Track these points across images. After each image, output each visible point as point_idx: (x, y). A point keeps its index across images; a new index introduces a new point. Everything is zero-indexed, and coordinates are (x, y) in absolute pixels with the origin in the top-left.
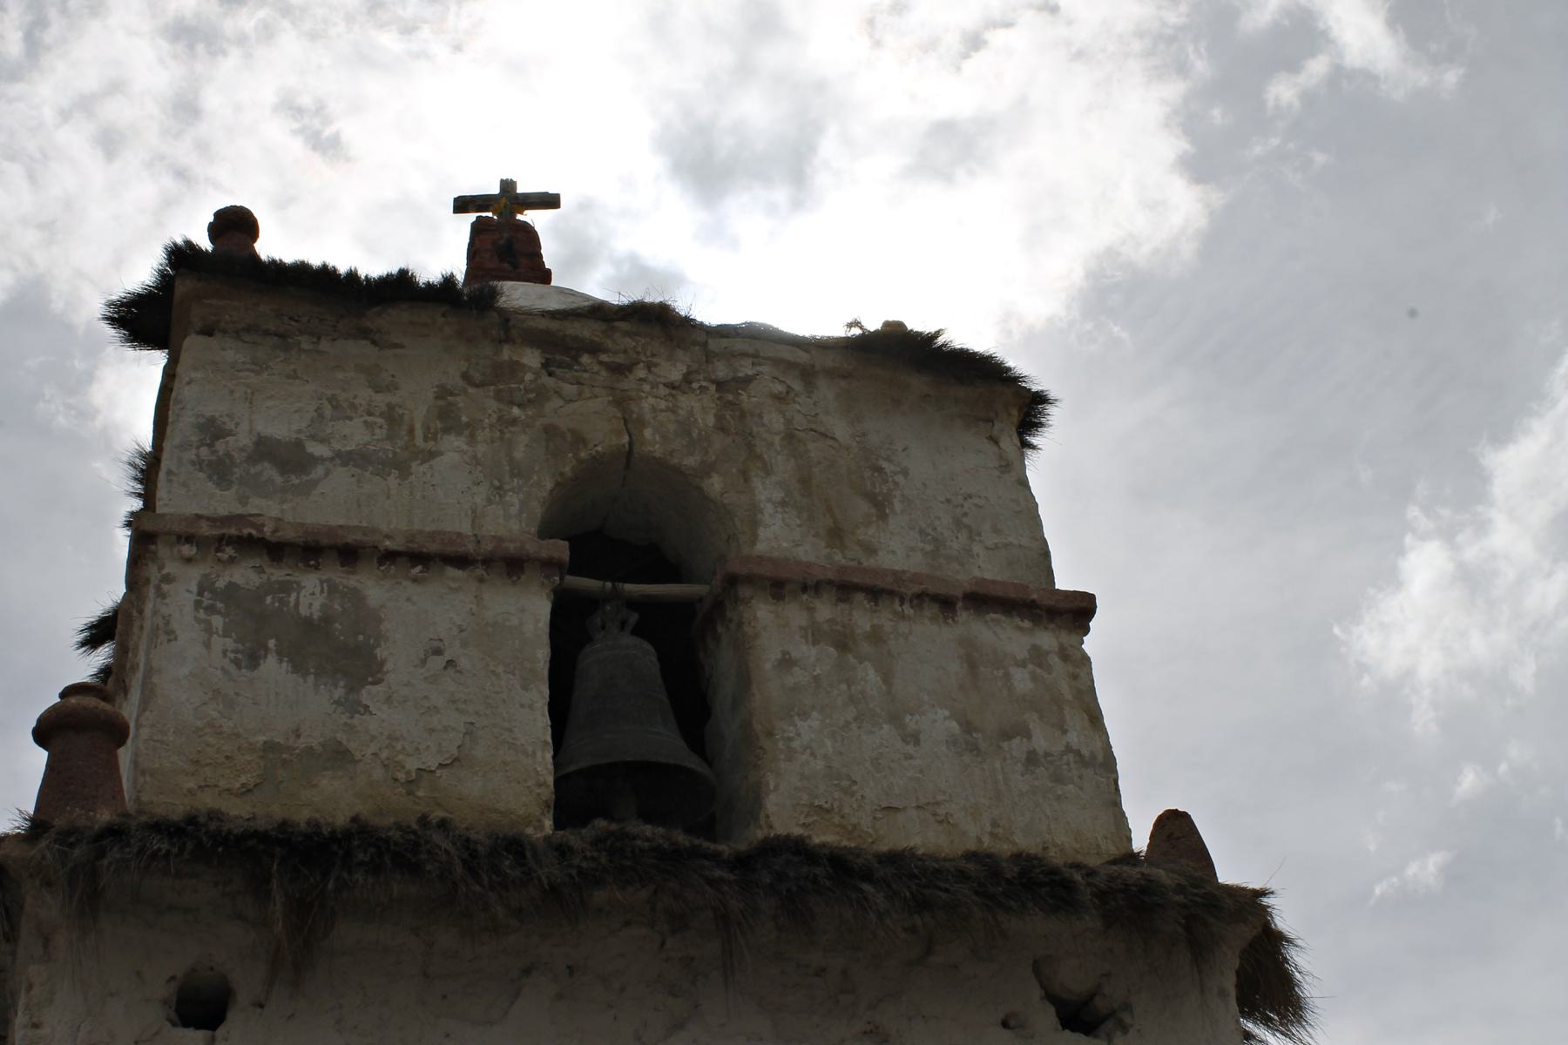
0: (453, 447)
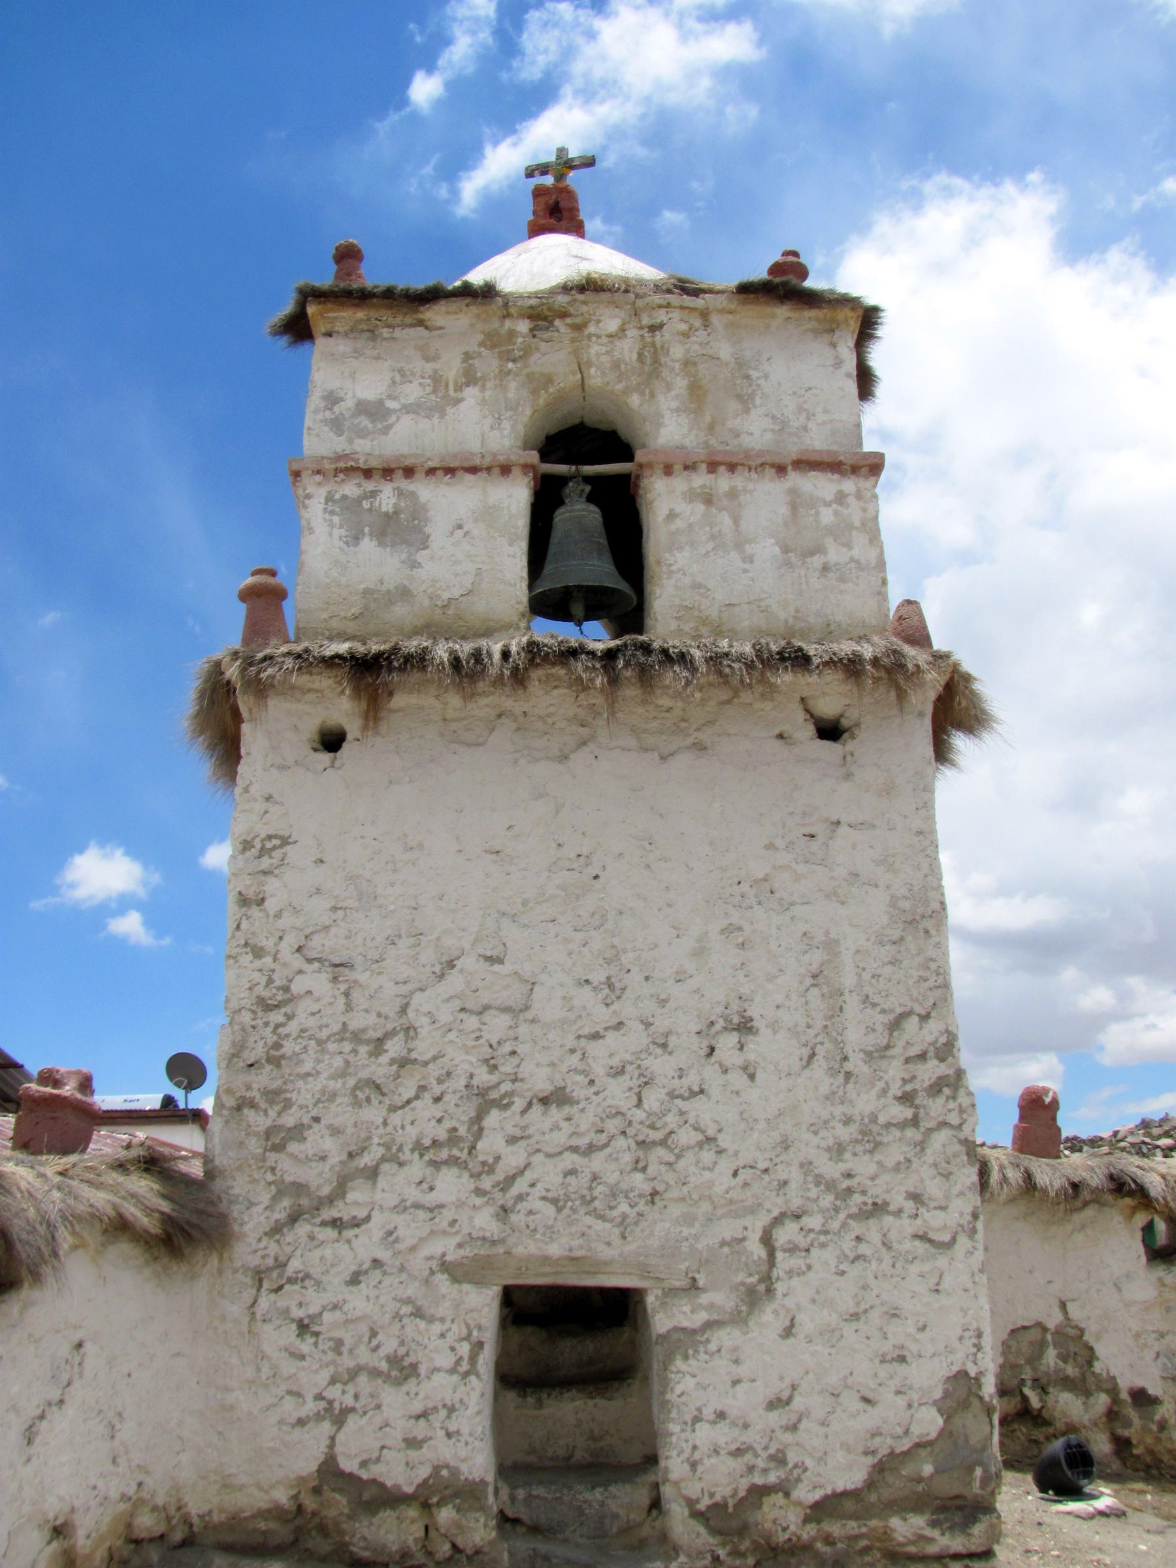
0: (471, 393)
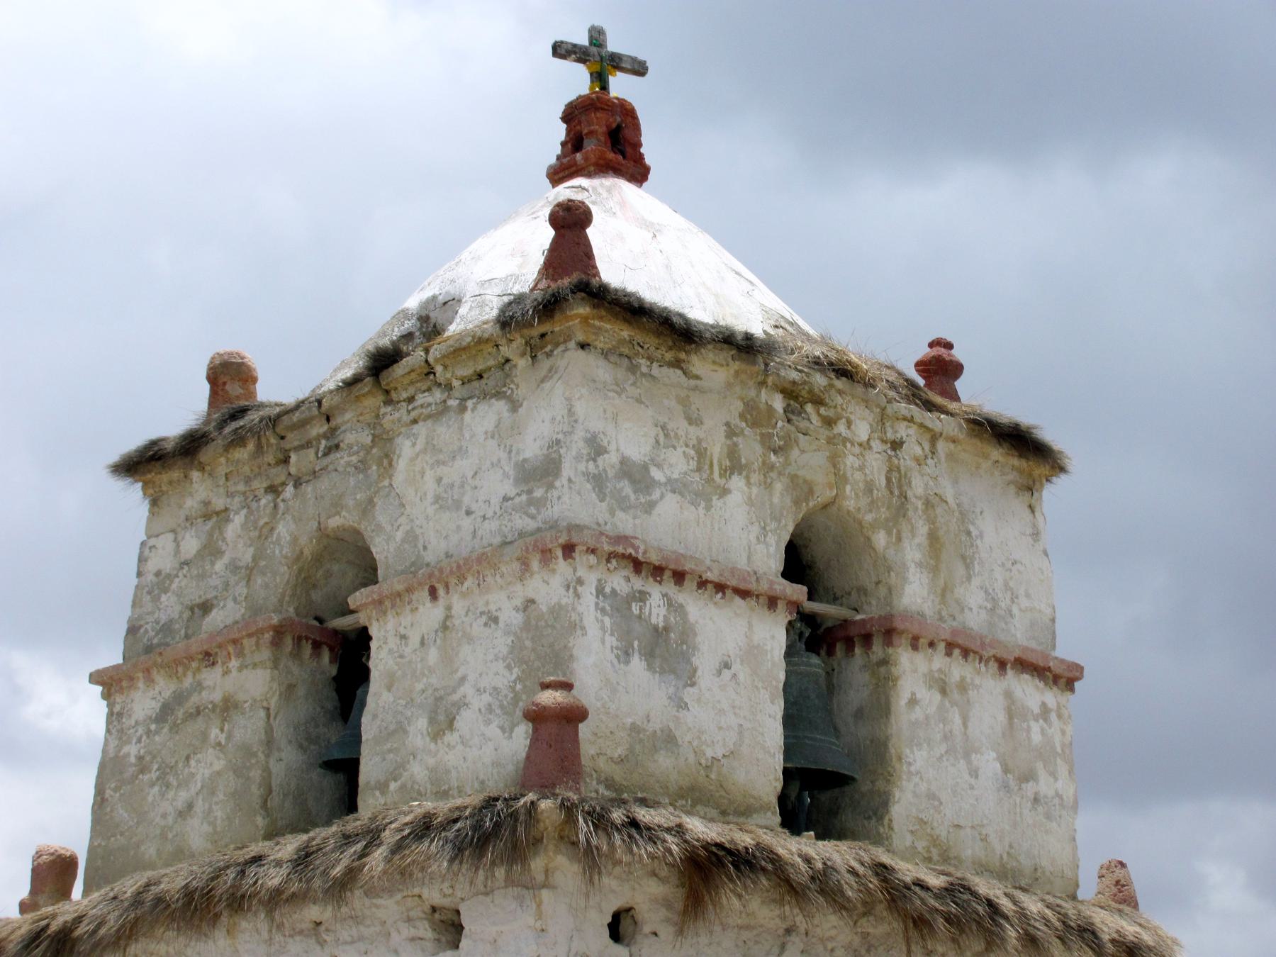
0: (737, 482)
